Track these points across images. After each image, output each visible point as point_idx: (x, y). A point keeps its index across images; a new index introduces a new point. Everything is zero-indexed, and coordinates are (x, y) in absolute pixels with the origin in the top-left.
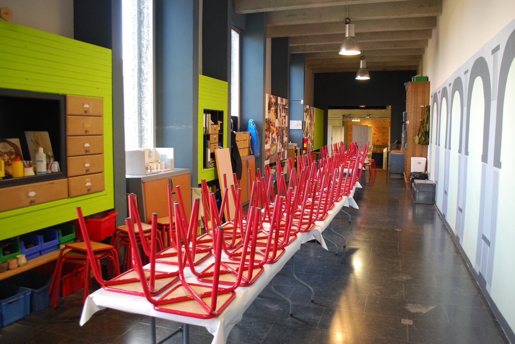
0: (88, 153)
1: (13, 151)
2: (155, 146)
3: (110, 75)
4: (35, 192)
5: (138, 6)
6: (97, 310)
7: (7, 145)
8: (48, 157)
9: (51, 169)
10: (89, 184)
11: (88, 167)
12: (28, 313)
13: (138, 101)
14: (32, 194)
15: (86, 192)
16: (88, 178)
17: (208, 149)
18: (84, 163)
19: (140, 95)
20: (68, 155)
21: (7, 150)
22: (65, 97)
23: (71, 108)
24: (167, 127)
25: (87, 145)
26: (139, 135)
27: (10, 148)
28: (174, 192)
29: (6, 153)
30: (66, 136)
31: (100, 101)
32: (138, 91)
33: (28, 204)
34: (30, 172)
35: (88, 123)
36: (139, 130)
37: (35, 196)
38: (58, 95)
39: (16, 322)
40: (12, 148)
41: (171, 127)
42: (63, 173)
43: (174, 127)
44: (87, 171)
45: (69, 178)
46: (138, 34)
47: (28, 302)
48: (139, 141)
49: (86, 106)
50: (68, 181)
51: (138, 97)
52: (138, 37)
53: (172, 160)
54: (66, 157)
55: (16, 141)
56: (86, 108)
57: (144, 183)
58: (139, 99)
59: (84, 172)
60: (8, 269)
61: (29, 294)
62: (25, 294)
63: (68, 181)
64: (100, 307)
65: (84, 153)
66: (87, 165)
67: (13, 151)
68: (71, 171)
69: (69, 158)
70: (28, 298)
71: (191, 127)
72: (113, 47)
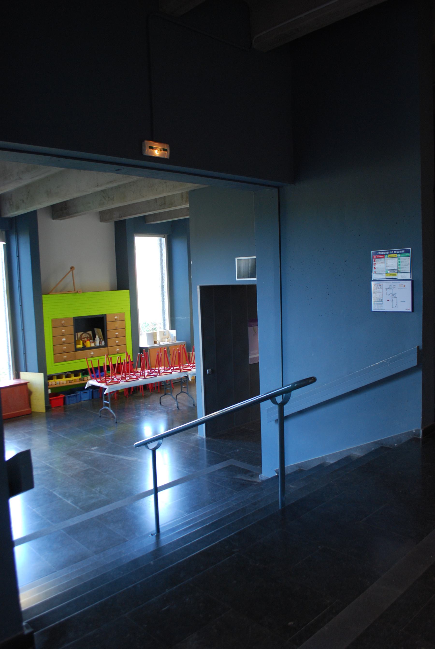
0: (117, 337)
1: (89, 336)
2: (170, 328)
3: (129, 301)
4: (94, 353)
5: (160, 251)
6: (90, 385)
7: (86, 334)
8: (100, 339)
9: (101, 343)
10: (118, 350)
11: (118, 343)
12: (91, 398)
13: (162, 304)
14: (92, 353)
15: (117, 353)
16: (117, 347)
17: (103, 344)
18: (116, 341)
19: (163, 300)
20: (108, 338)
21: (86, 336)
22: (106, 315)
23: (108, 319)
24: (177, 318)
25: (117, 333)
26: (163, 322)
27: (88, 335)
28: (170, 354)
29: (86, 337)
30: (107, 331)
31: (123, 314)
32: (162, 298)
33: (91, 357)
34: (93, 345)
35: (117, 324)
36: (163, 320)
37: (93, 354)
38: (103, 315)
39: (86, 400)
40: (88, 335)
41: (178, 318)
42: (106, 345)
43: (180, 318)
44: (117, 344)
45: (108, 347)
46: (161, 267)
47: (91, 394)
48: (163, 325)
49: (116, 317)
50: (108, 348)
51: (162, 302)
52: (161, 269)
53: (175, 337)
54: (107, 339)
55: (90, 332)
56: (116, 318)
57: (149, 349)
58: (163, 303)
59: (116, 345)
60: (84, 380)
61: (91, 391)
62: (90, 391)
63: (108, 348)
64: (91, 384)
65: (115, 337)
66: (117, 342)
67: (89, 336)
68: (109, 344)
69: (108, 339)
70: (91, 393)
71: (189, 318)
72: (130, 288)
